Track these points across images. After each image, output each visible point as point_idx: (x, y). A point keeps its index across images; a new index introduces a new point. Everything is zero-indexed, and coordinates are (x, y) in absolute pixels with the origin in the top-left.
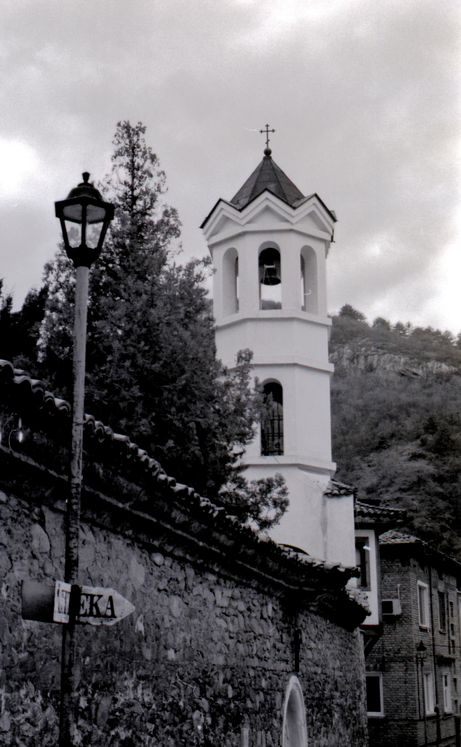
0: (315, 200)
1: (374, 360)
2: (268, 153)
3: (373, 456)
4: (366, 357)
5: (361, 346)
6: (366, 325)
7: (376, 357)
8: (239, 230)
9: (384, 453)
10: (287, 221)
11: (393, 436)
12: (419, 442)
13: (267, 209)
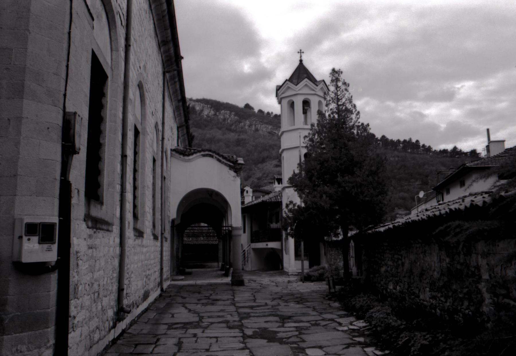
0: (323, 83)
1: (259, 127)
2: (301, 61)
3: (260, 165)
4: (255, 125)
5: (253, 121)
6: (255, 112)
7: (259, 126)
8: (295, 93)
9: (265, 164)
10: (314, 90)
11: (267, 157)
12: (278, 160)
13: (306, 85)
